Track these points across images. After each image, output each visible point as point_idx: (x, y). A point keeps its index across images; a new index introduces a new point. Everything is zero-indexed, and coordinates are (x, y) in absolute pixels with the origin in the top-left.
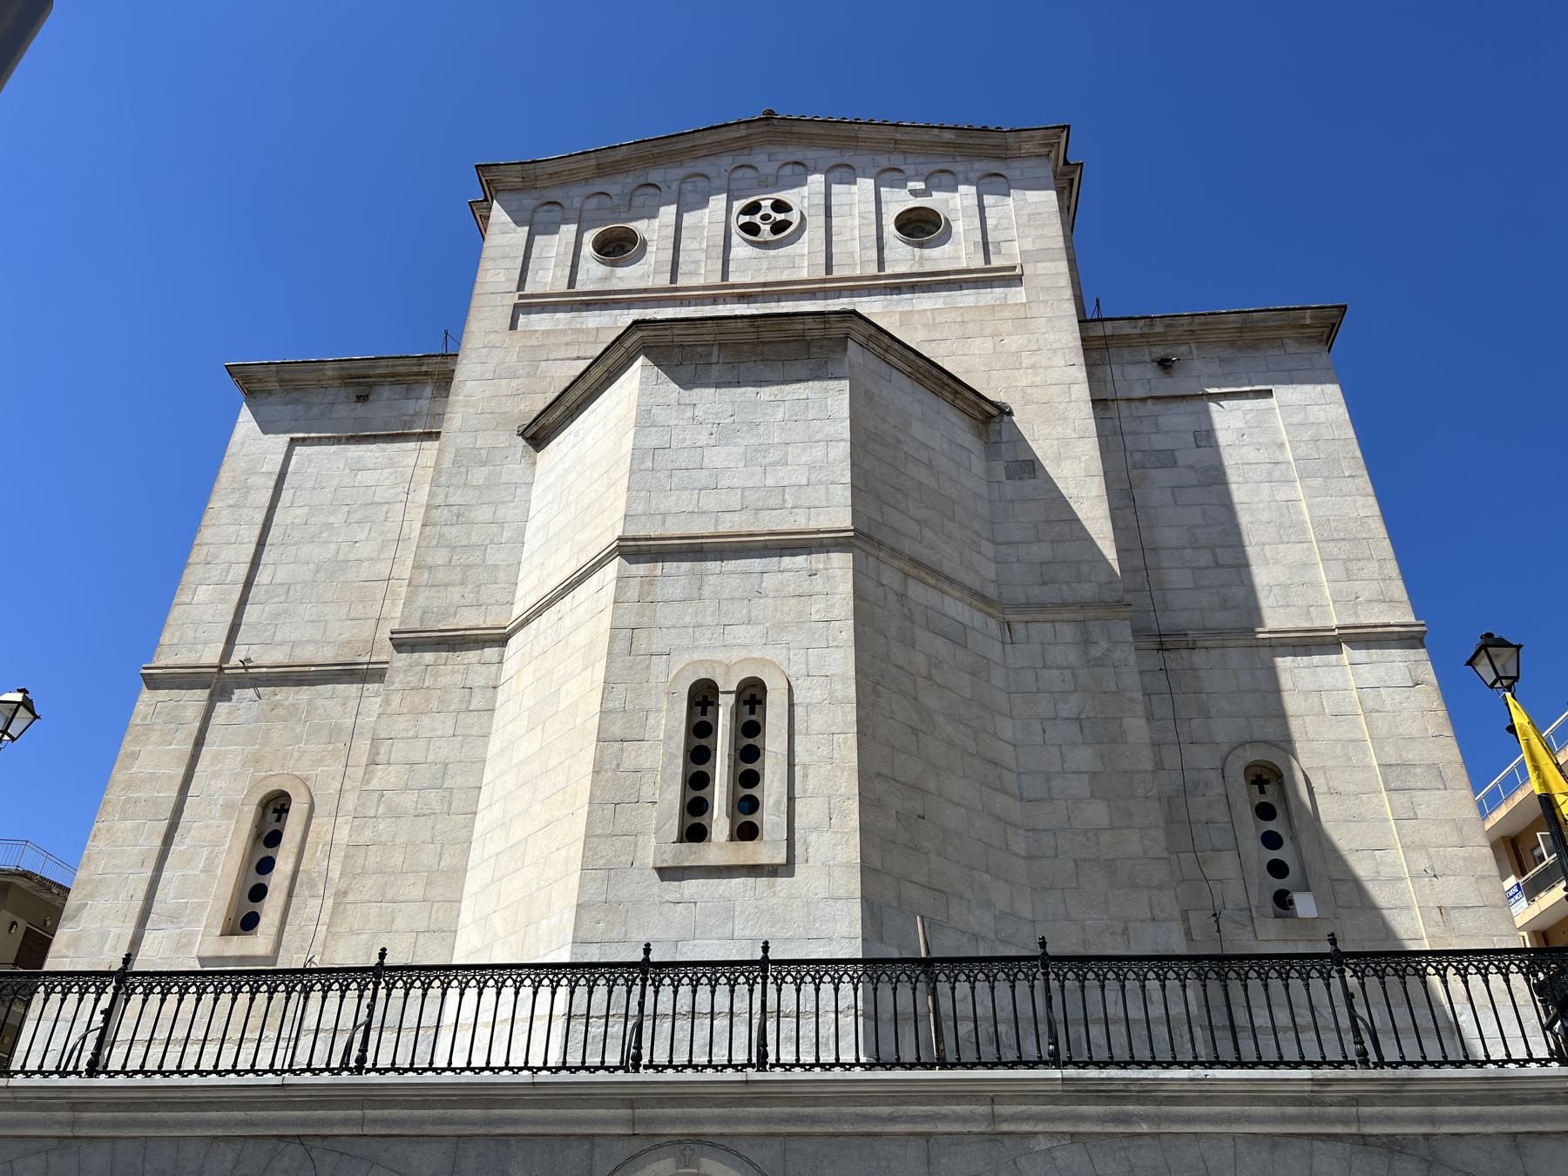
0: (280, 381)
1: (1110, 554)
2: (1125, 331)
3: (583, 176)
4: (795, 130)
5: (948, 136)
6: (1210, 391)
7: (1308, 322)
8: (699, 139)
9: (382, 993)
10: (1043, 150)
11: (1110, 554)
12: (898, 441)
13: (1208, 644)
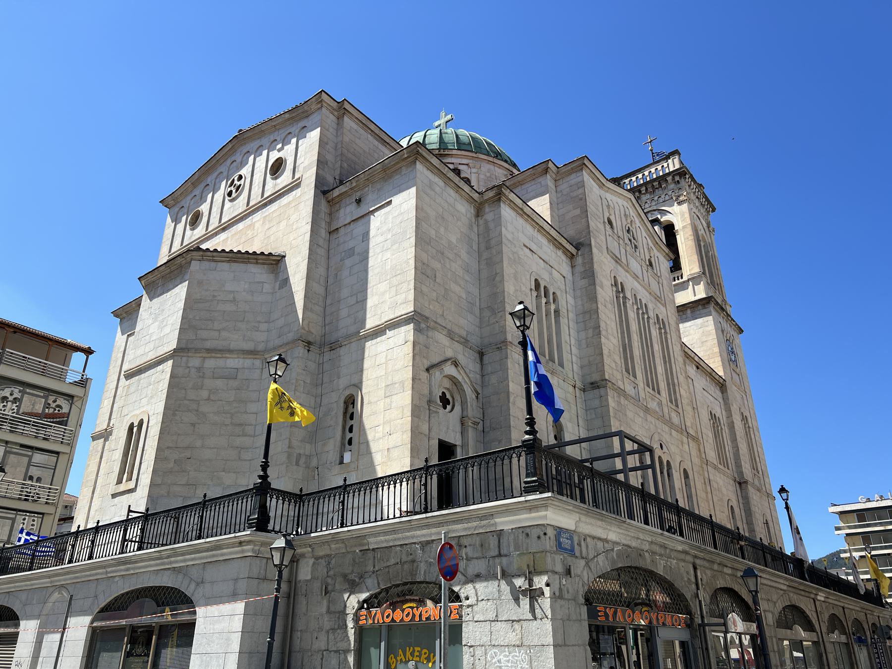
0: (126, 312)
1: (300, 316)
2: (345, 190)
3: (190, 190)
4: (245, 137)
5: (287, 116)
6: (371, 209)
7: (406, 156)
8: (218, 157)
9: (346, 496)
10: (319, 106)
11: (300, 316)
12: (214, 296)
13: (345, 343)
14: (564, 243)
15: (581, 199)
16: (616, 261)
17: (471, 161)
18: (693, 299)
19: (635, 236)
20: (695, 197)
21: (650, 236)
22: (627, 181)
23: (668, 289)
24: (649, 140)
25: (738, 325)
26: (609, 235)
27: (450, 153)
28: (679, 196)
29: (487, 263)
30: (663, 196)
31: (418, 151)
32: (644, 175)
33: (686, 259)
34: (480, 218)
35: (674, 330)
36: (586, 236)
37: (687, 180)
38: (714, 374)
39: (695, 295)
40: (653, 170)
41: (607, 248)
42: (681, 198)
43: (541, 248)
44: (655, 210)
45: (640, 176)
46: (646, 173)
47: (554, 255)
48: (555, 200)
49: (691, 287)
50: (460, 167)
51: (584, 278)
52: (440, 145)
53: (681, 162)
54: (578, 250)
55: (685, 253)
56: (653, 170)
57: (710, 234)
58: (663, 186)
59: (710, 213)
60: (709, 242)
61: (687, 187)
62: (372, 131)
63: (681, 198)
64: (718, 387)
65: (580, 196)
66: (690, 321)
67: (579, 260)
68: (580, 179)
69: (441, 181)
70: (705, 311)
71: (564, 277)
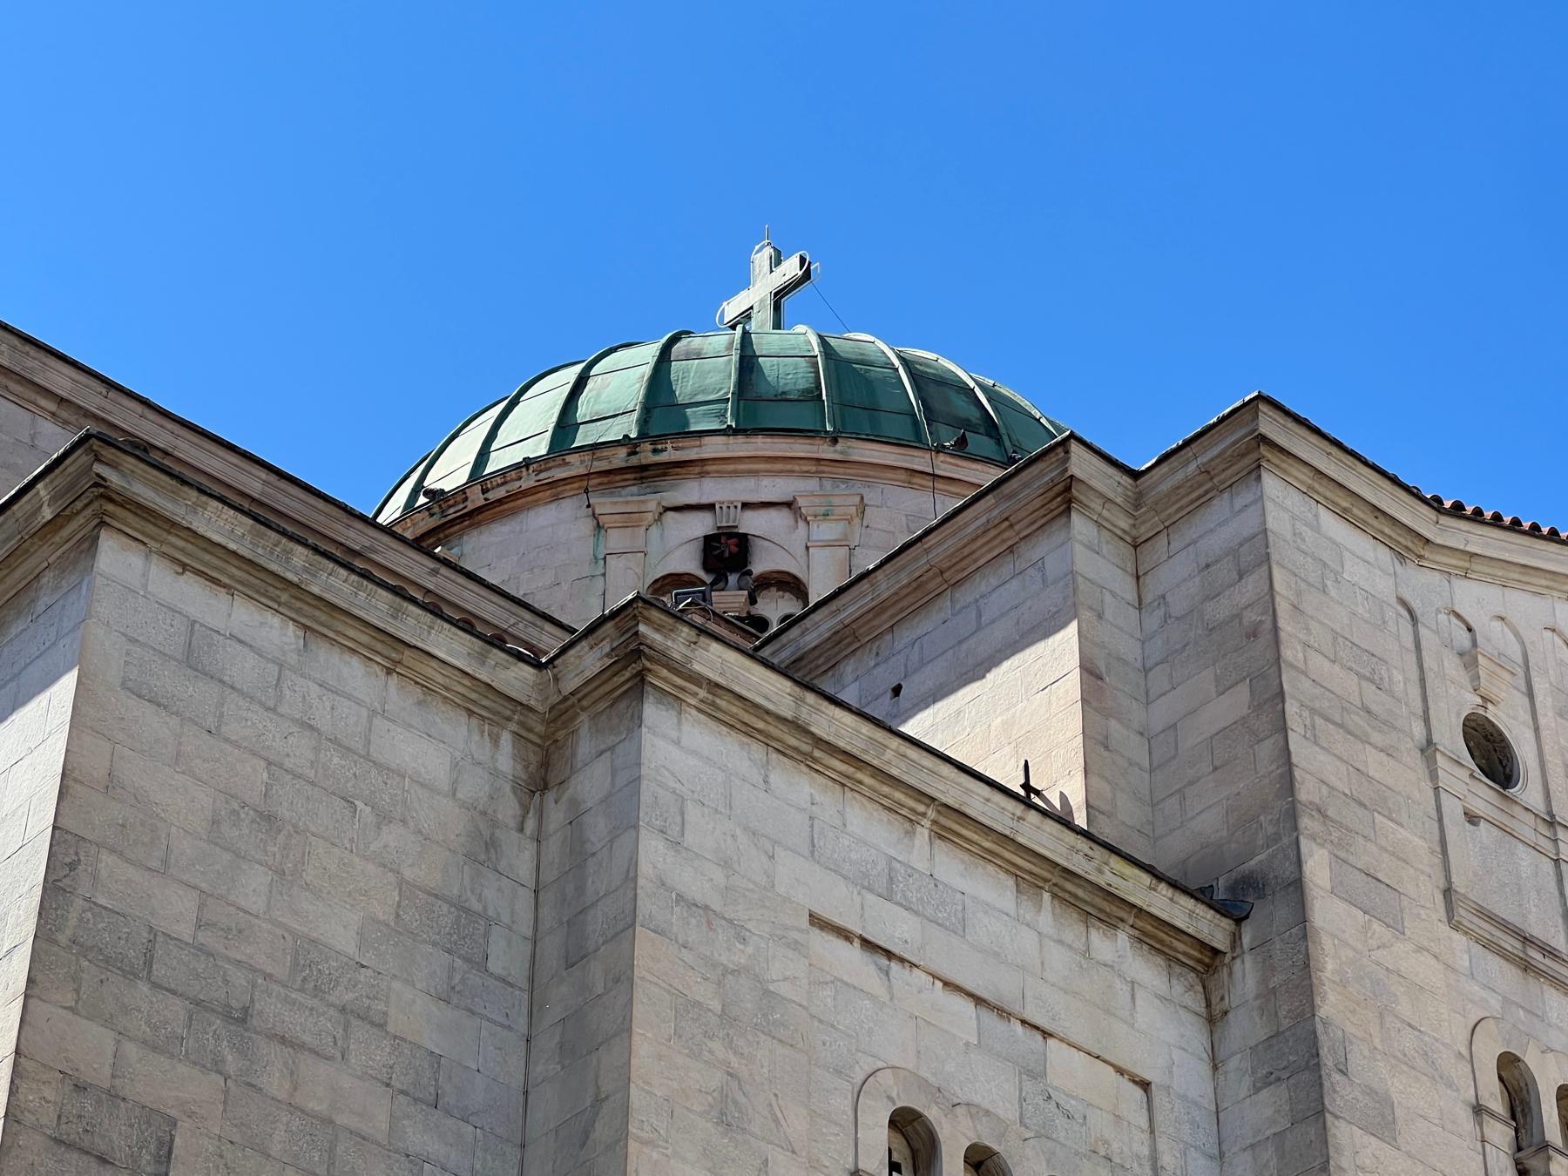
7: (47, 514)
14: (1135, 887)
15: (1253, 634)
16: (1527, 967)
17: (812, 484)
26: (1472, 819)
27: (692, 455)
29: (561, 1046)
31: (100, 483)
34: (550, 796)
36: (1277, 838)
41: (1448, 892)
43: (960, 928)
47: (1059, 959)
48: (1129, 648)
50: (751, 523)
51: (1268, 1081)
52: (644, 422)
54: (1239, 921)
62: (62, 401)
65: (1250, 617)
67: (1245, 978)
68: (1245, 525)
69: (276, 621)
71: (1145, 1085)
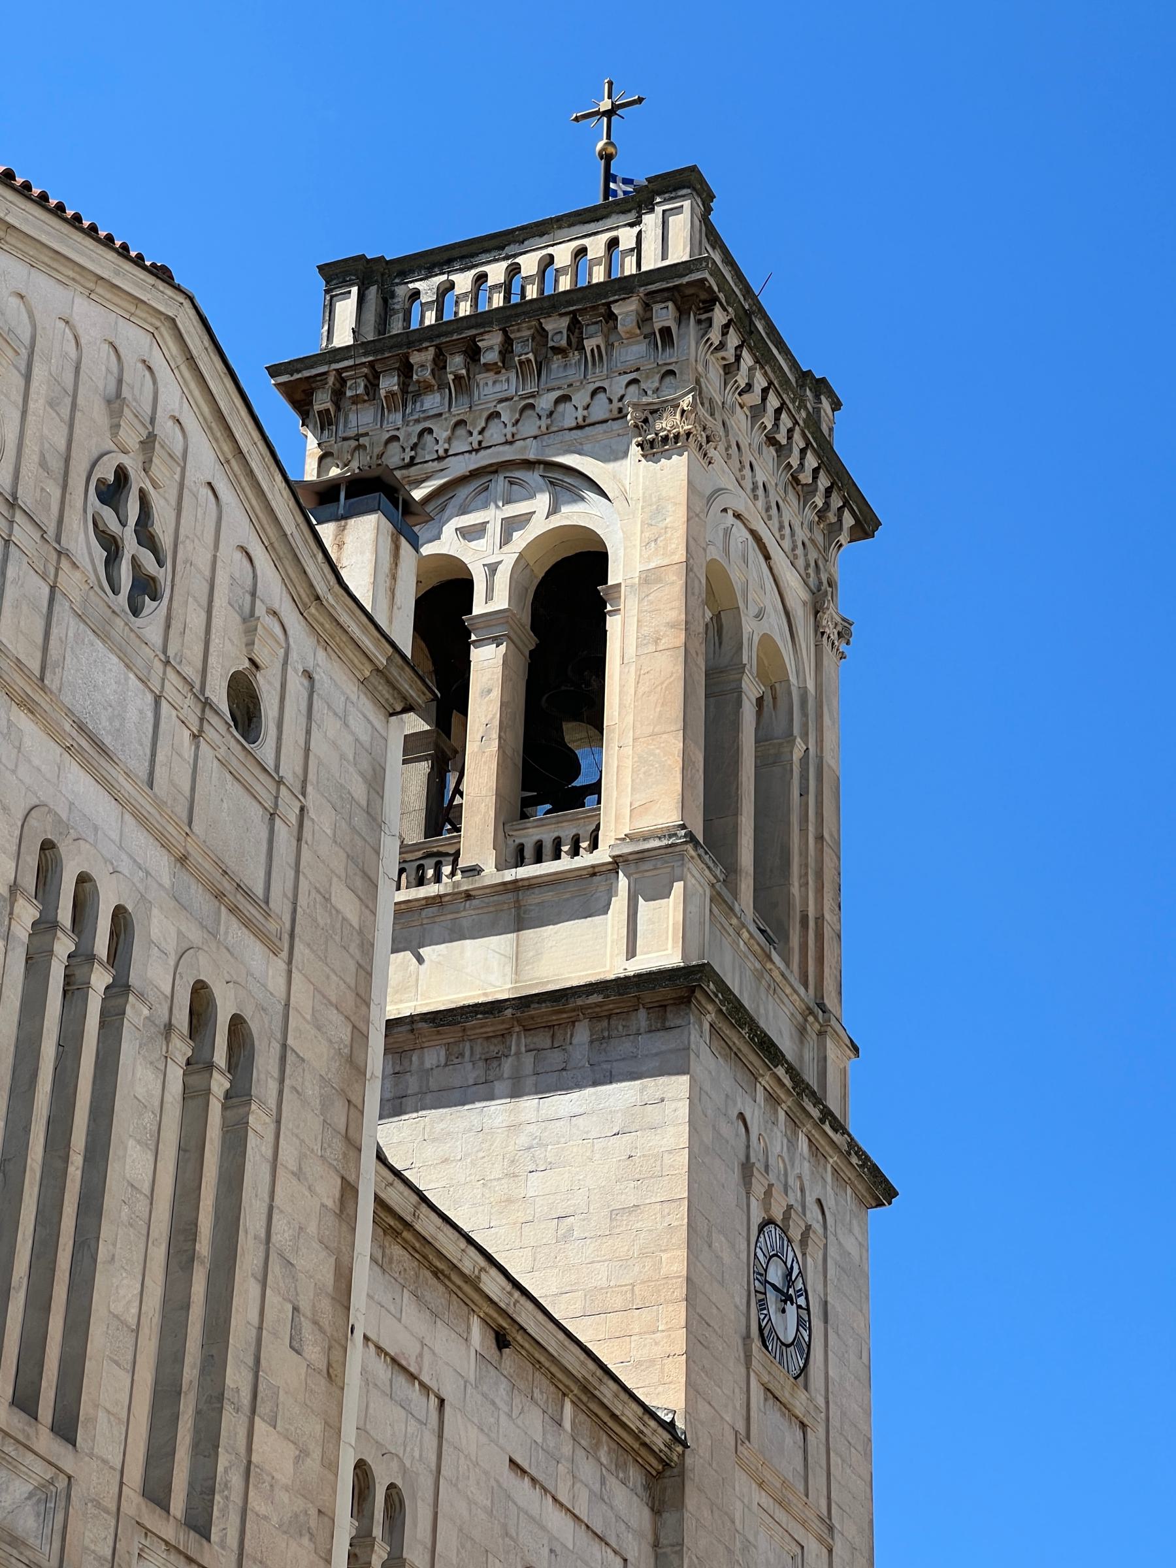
18: (615, 966)
19: (162, 527)
20: (759, 438)
21: (281, 549)
22: (427, 288)
23: (338, 862)
24: (606, 105)
25: (865, 1159)
28: (656, 412)
30: (580, 398)
32: (514, 270)
33: (628, 751)
35: (312, 1090)
37: (715, 336)
38: (607, 1392)
39: (631, 953)
40: (563, 254)
42: (667, 424)
44: (529, 464)
45: (496, 272)
46: (529, 263)
49: (619, 903)
53: (707, 232)
55: (630, 718)
56: (563, 254)
57: (818, 647)
58: (589, 344)
59: (844, 538)
60: (804, 692)
61: (714, 375)
63: (667, 424)
64: (635, 1475)
66: (579, 1086)
70: (661, 1042)
